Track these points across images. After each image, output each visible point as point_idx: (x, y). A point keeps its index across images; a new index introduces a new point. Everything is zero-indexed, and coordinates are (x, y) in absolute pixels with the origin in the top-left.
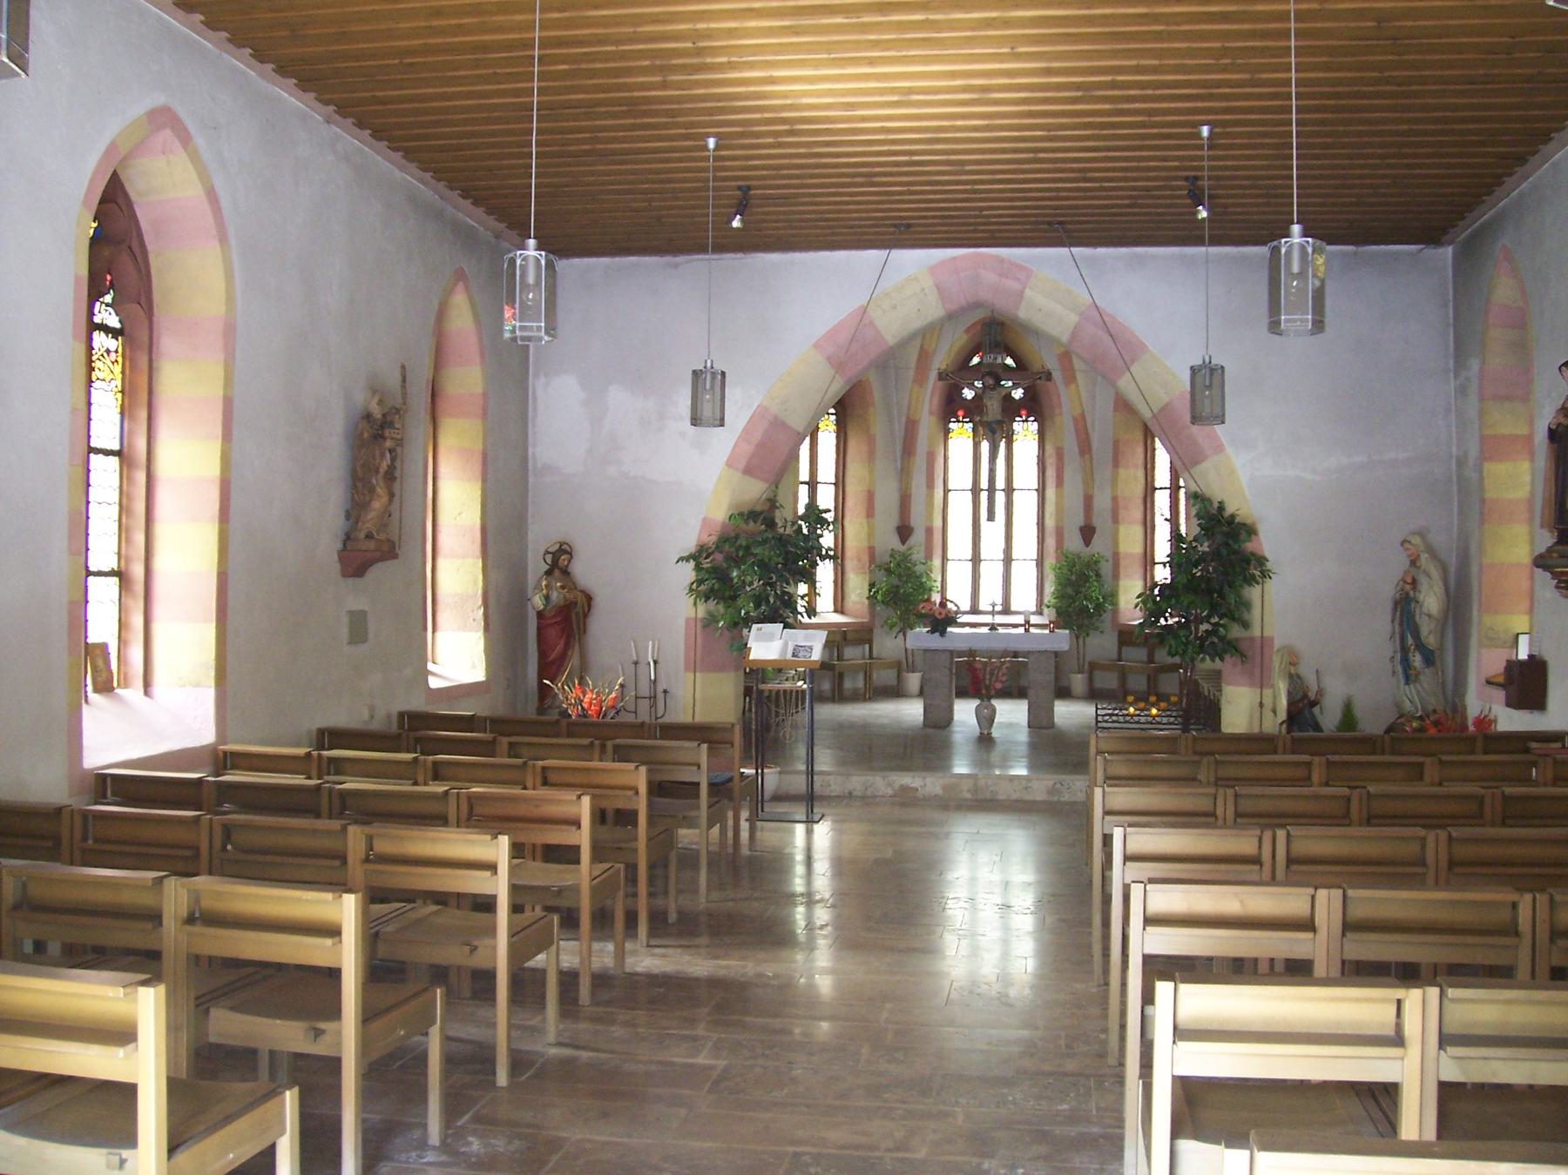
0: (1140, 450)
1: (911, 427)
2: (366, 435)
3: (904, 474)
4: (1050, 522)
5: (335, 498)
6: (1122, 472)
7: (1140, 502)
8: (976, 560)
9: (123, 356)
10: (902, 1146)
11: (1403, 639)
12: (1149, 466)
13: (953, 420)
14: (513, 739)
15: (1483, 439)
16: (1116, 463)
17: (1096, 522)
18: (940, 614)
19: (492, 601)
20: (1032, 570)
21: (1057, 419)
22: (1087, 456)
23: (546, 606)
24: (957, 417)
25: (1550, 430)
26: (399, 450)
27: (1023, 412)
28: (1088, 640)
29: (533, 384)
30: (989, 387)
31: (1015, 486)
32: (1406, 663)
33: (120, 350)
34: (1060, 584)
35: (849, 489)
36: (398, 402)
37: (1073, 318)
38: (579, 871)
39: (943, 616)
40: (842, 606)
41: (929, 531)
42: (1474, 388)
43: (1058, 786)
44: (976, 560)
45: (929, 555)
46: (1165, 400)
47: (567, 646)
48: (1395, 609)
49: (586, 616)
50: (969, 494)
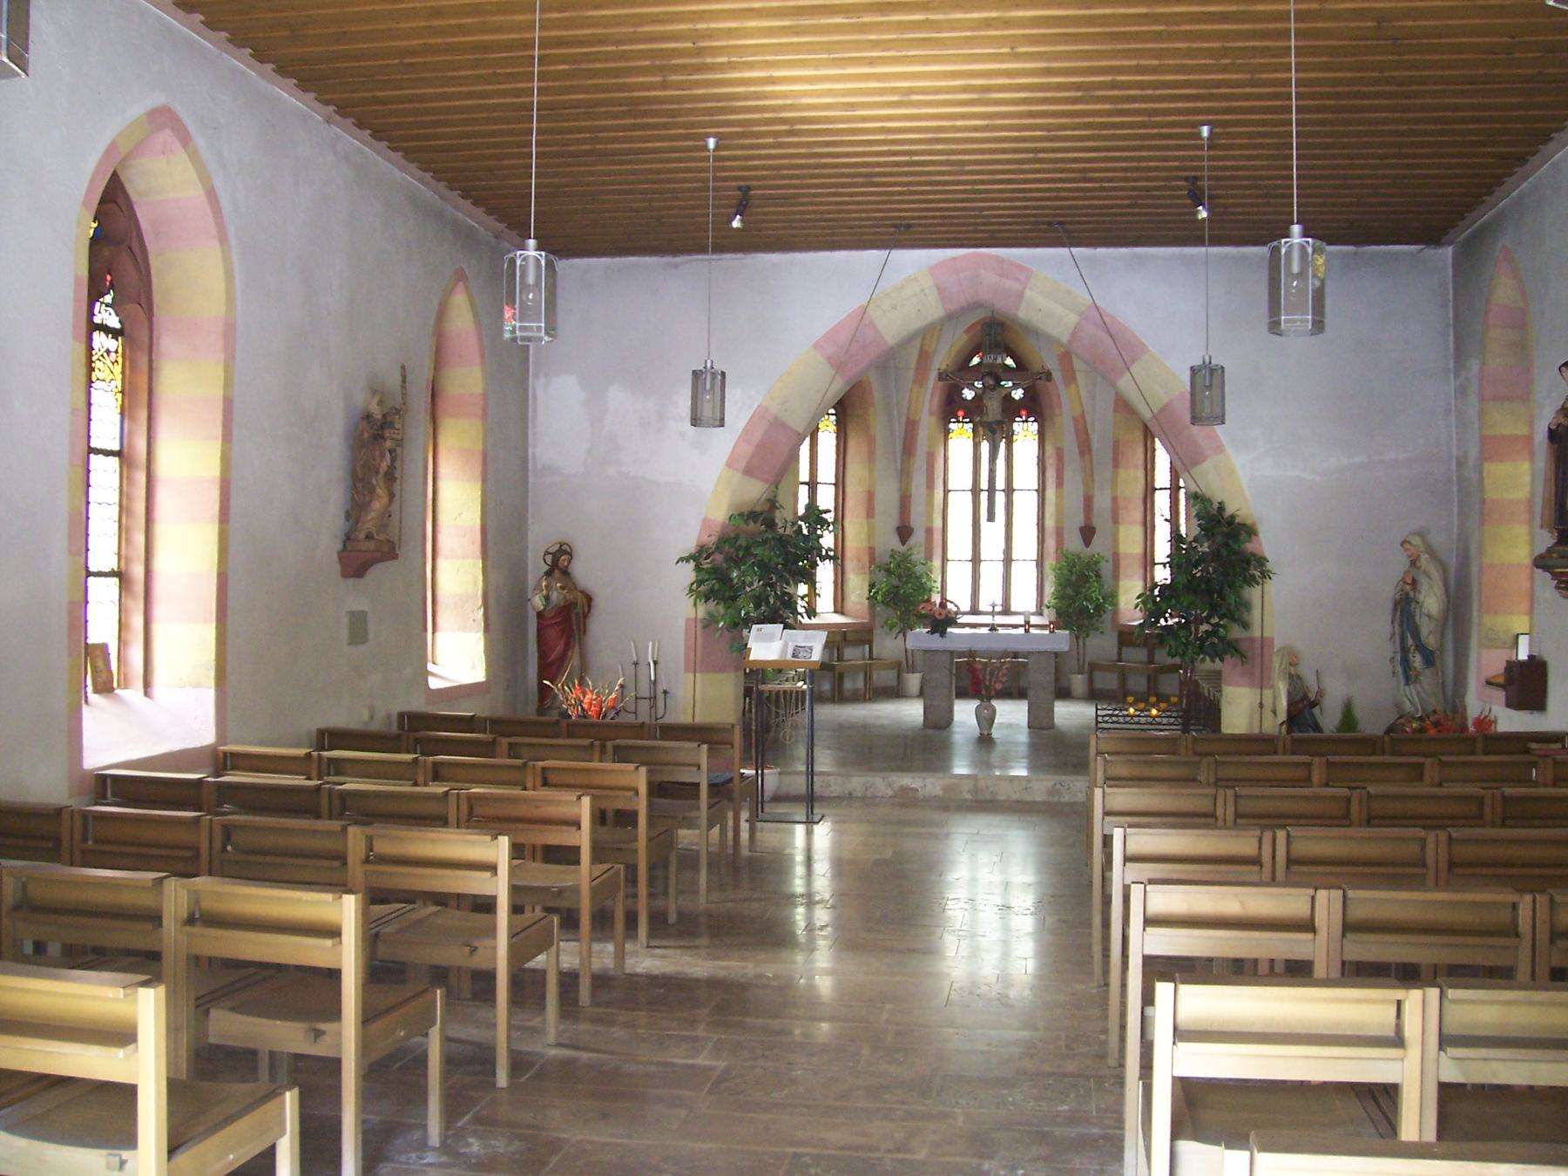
0: (1140, 450)
1: (911, 428)
2: (366, 435)
3: (904, 474)
4: (1050, 523)
5: (335, 498)
6: (1122, 472)
7: (1140, 503)
8: (976, 560)
9: (123, 357)
10: (902, 1147)
11: (1403, 639)
12: (1149, 466)
13: (953, 420)
14: (513, 740)
15: (1483, 440)
16: (1116, 464)
17: (1096, 522)
18: (940, 614)
19: (492, 602)
20: (1032, 570)
21: (1057, 420)
22: (1087, 457)
23: (546, 606)
24: (957, 417)
25: (1550, 430)
26: (399, 450)
27: (1023, 413)
28: (1088, 641)
29: (533, 384)
30: (989, 388)
31: (1015, 487)
32: (1406, 663)
33: (120, 350)
34: (1060, 585)
35: (849, 489)
36: (398, 403)
37: (1073, 319)
38: (579, 872)
39: (943, 617)
40: (842, 607)
41: (929, 532)
42: (1474, 388)
43: (1058, 786)
44: (976, 560)
45: (929, 556)
46: (1165, 400)
47: (567, 647)
48: (1395, 610)
49: (586, 616)
50: (969, 495)
